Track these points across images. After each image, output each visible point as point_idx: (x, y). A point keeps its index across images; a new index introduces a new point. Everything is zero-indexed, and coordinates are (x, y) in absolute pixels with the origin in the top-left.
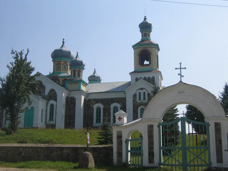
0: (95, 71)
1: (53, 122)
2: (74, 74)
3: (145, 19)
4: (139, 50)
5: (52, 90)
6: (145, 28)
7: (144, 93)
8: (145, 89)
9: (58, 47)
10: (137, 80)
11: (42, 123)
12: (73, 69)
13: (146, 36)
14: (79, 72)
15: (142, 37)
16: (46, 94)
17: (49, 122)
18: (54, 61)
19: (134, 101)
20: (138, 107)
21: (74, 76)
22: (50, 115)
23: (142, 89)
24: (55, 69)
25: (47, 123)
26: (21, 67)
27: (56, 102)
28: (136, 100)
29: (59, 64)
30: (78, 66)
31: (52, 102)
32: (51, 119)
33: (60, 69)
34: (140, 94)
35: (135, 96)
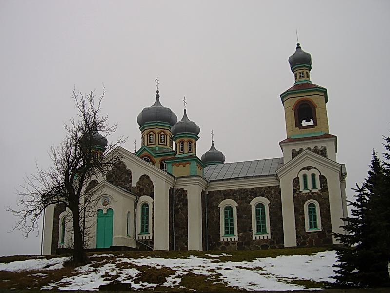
1: (149, 235)
3: (299, 47)
4: (293, 101)
5: (145, 178)
6: (301, 62)
7: (313, 175)
8: (315, 168)
10: (294, 154)
11: (128, 238)
13: (303, 77)
14: (190, 143)
15: (296, 78)
16: (134, 184)
18: (143, 128)
19: (294, 191)
20: (304, 201)
21: (182, 152)
22: (143, 222)
23: (308, 168)
24: (146, 142)
25: (137, 239)
26: (89, 143)
27: (153, 198)
28: (299, 189)
29: (162, 133)
30: (190, 132)
31: (145, 198)
32: (145, 229)
33: (154, 143)
34: (305, 176)
35: (296, 181)
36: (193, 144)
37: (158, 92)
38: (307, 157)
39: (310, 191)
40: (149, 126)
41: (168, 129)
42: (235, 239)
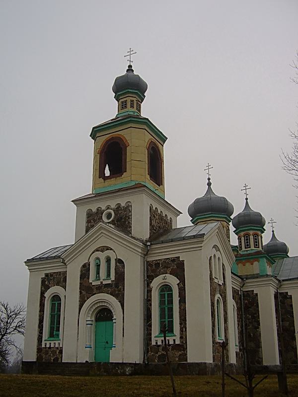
3: (130, 70)
4: (102, 140)
6: (129, 88)
7: (108, 260)
14: (256, 237)
17: (48, 343)
21: (248, 246)
23: (103, 249)
32: (55, 330)
35: (85, 269)
36: (259, 237)
37: (209, 179)
38: (102, 232)
39: (102, 283)
40: (202, 218)
41: (225, 220)
42: (174, 340)
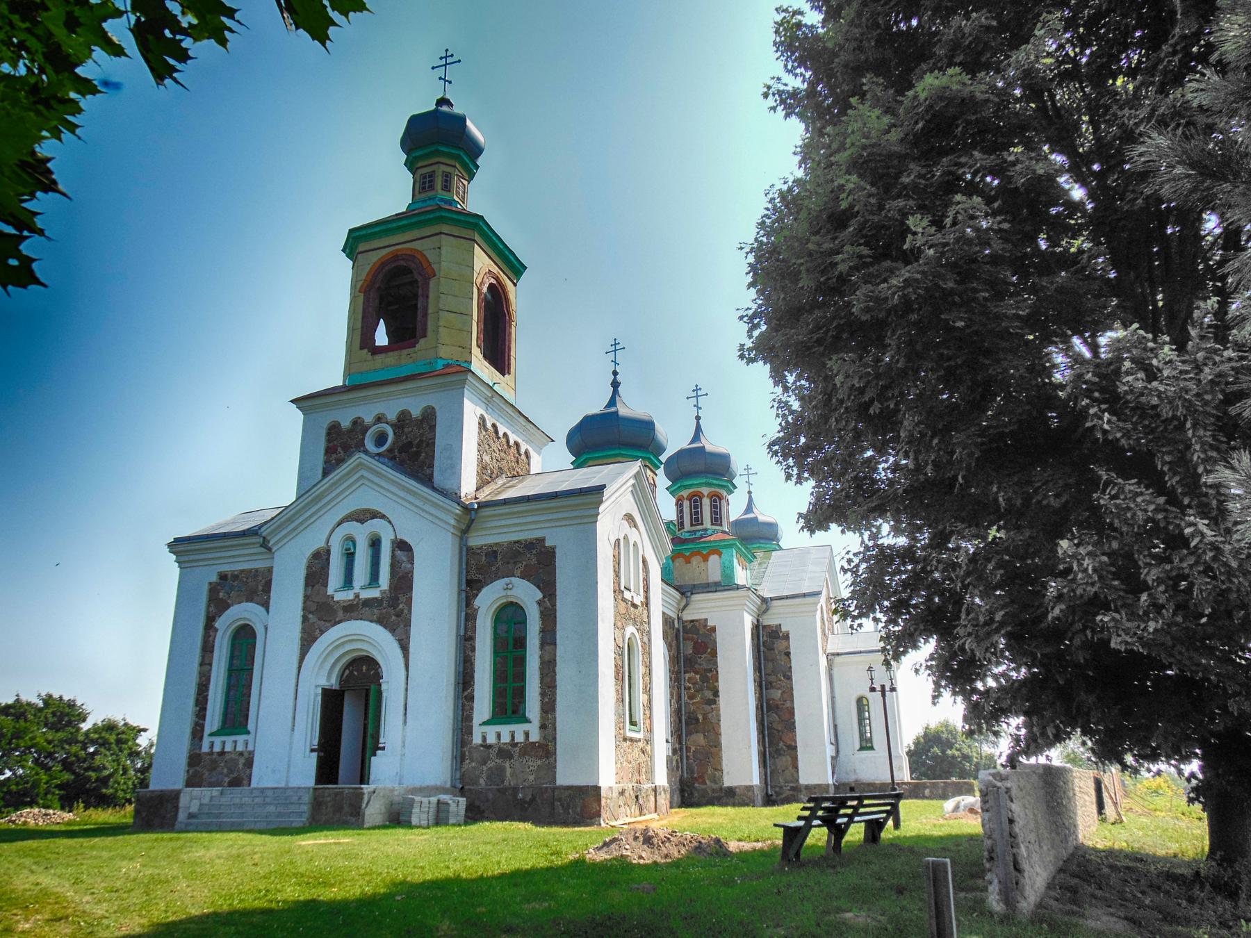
0: (750, 500)
2: (696, 513)
7: (375, 544)
9: (597, 406)
12: (685, 493)
13: (432, 187)
21: (697, 519)
23: (362, 516)
35: (319, 561)
